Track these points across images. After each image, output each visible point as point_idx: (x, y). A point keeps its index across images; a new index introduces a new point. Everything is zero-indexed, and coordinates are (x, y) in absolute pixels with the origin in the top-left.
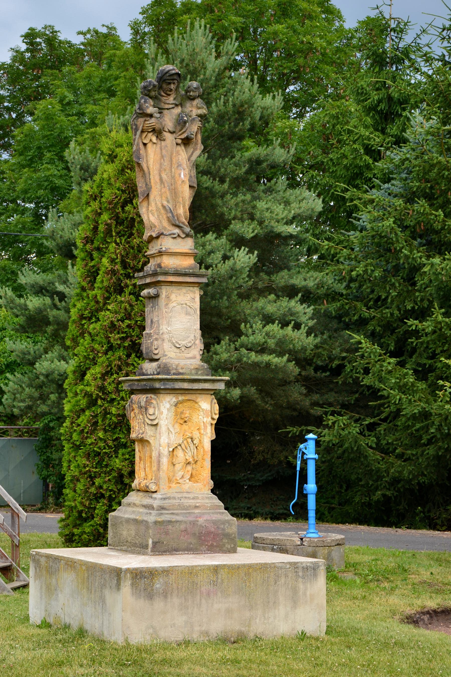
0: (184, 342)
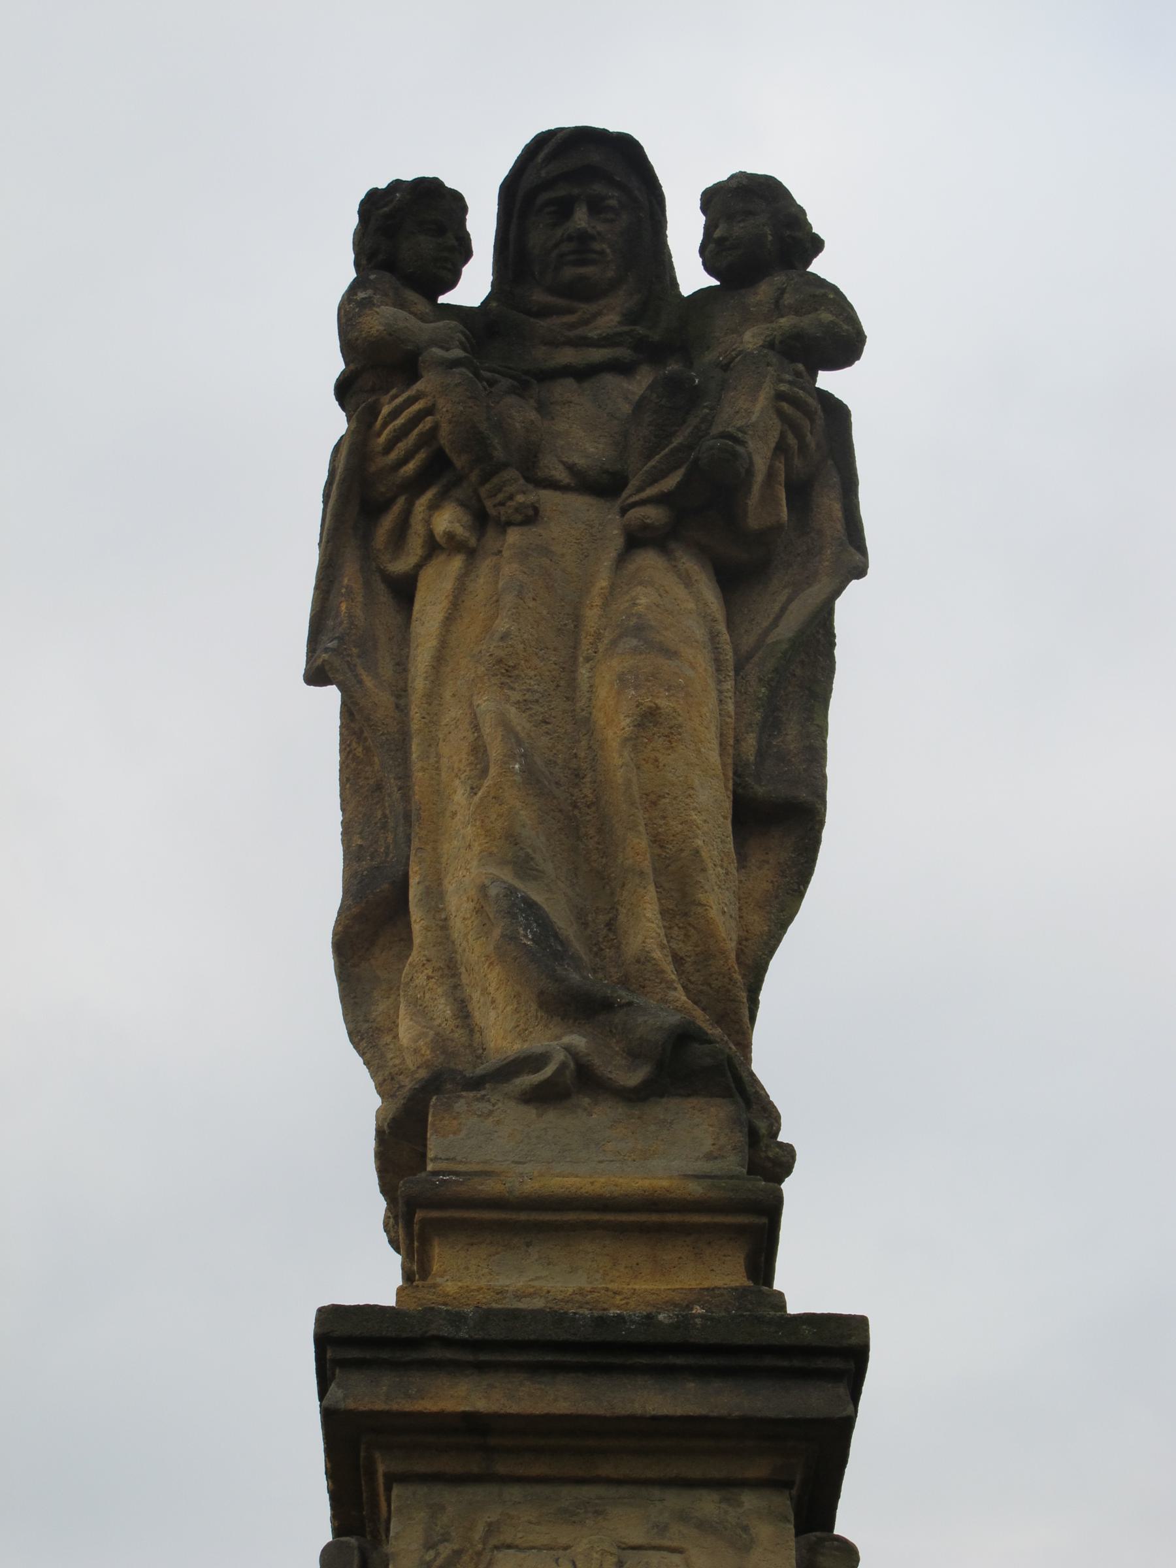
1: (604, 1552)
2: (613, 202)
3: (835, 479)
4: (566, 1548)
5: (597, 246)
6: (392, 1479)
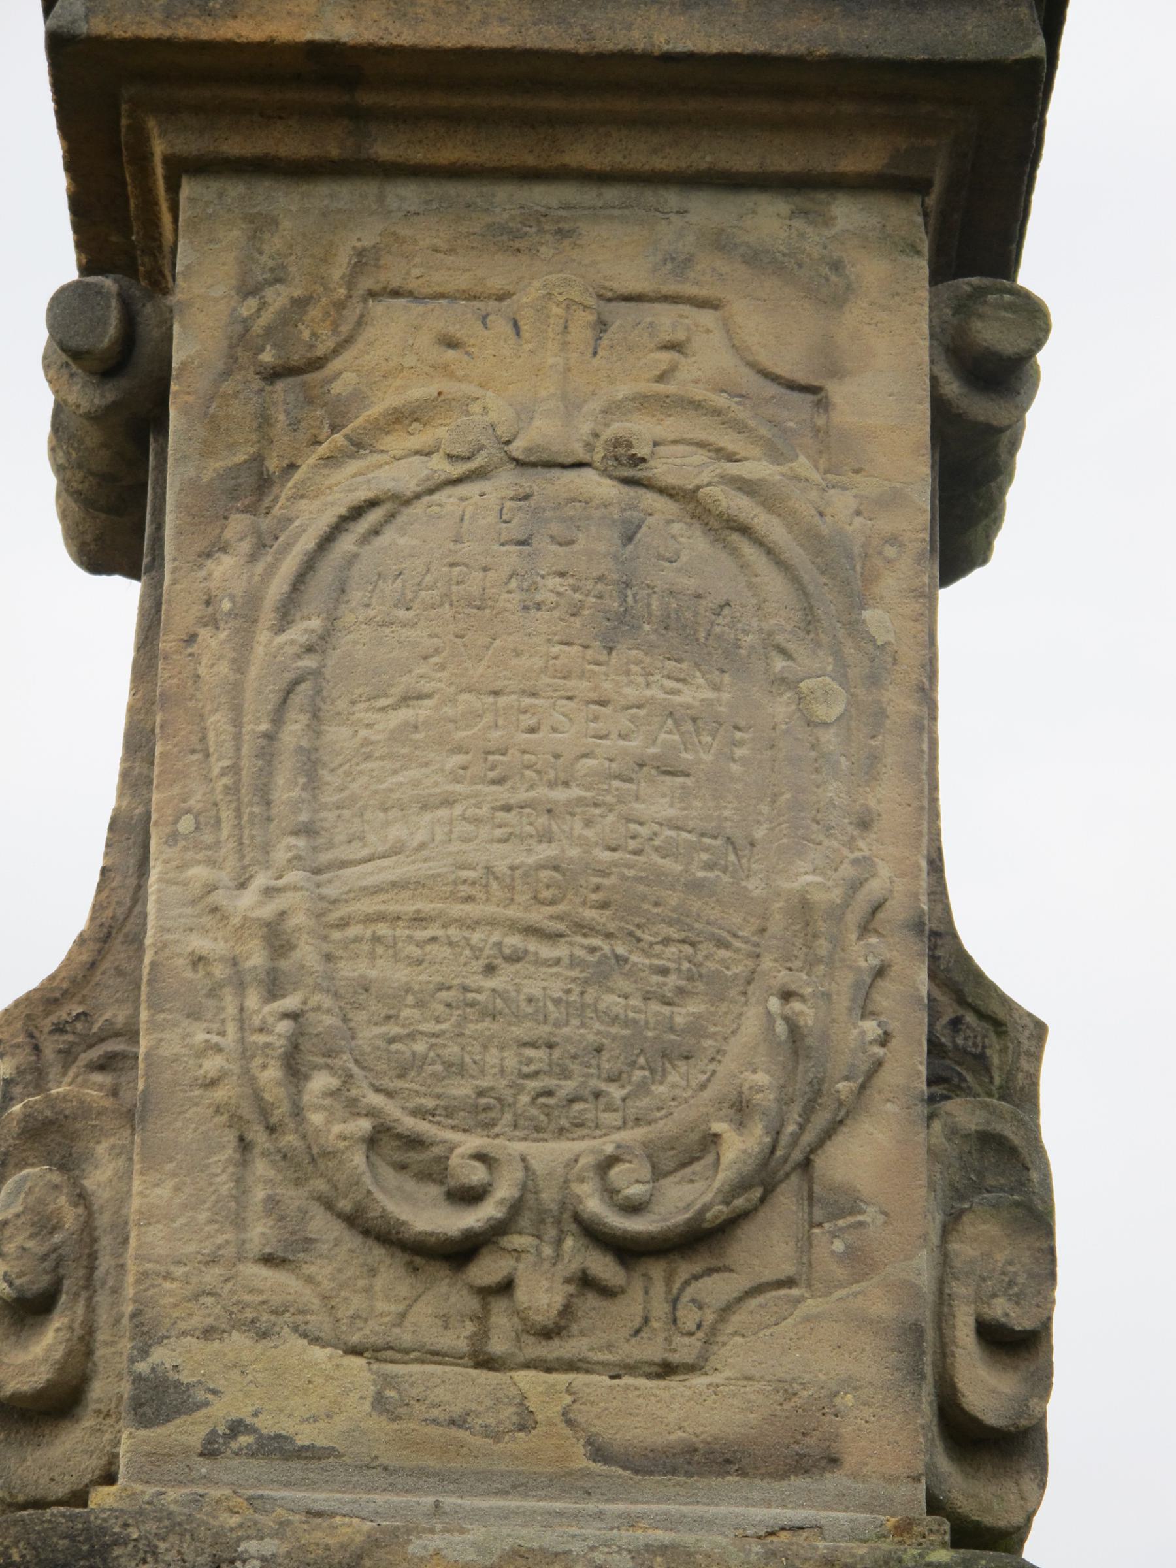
0: (548, 1153)
1: (570, 304)
4: (501, 298)
6: (179, 168)
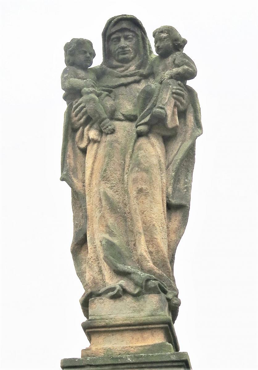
2: (130, 37)
3: (192, 110)
5: (128, 49)
